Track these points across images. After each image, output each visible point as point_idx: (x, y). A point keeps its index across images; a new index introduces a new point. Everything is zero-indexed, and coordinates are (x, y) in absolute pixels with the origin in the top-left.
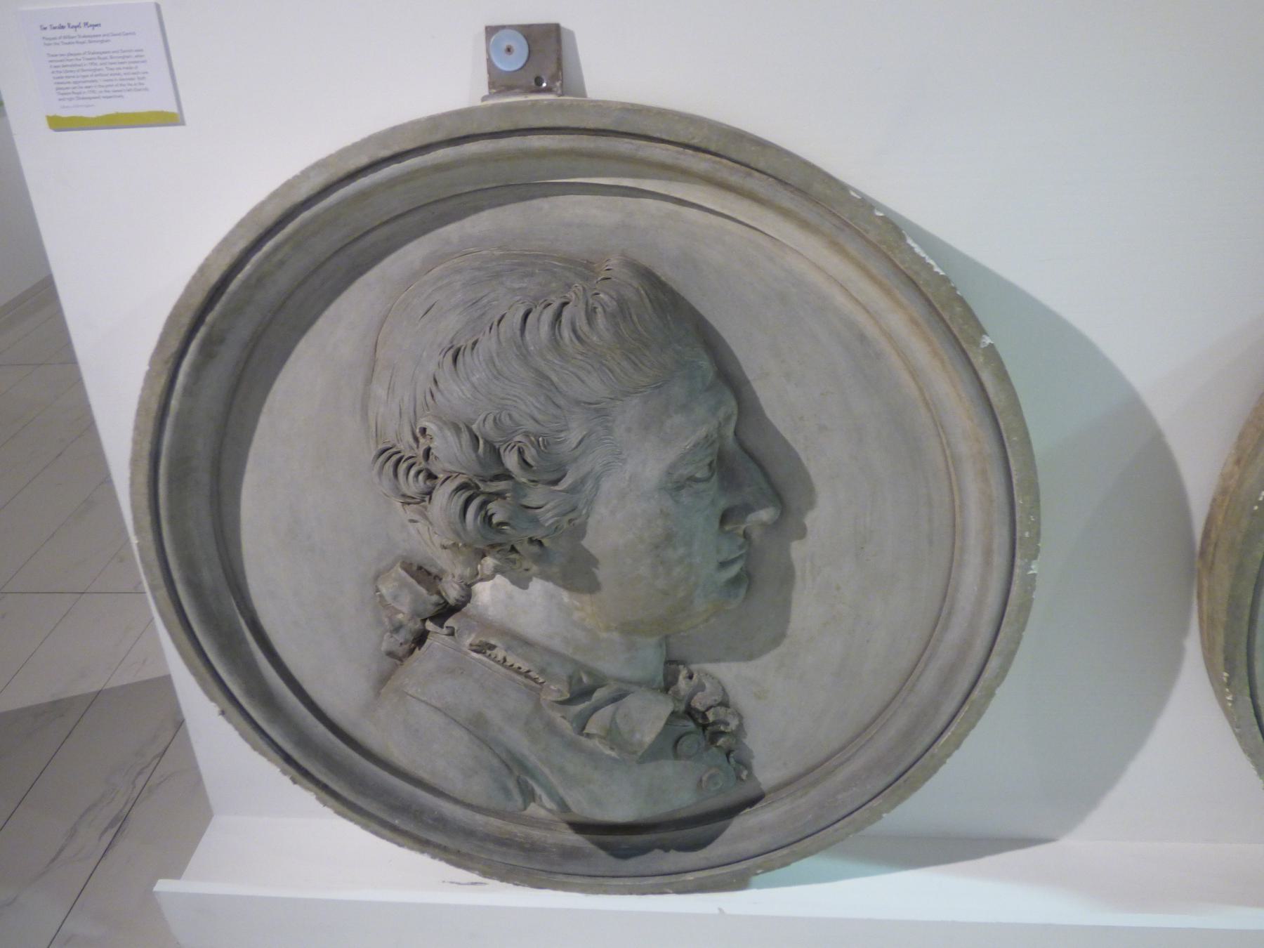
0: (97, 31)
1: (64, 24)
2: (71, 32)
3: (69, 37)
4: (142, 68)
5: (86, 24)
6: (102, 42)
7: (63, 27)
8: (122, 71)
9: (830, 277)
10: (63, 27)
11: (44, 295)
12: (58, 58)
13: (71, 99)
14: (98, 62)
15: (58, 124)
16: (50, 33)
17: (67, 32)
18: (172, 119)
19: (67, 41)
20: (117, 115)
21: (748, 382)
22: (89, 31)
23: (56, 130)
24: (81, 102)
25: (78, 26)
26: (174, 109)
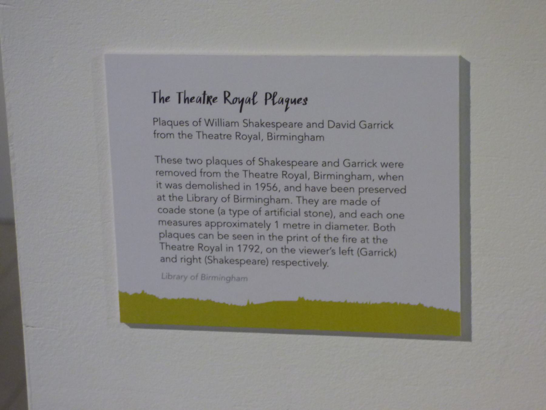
0: (296, 113)
1: (216, 92)
2: (230, 112)
3: (220, 123)
4: (390, 203)
5: (271, 97)
6: (302, 139)
7: (209, 100)
8: (337, 209)
9: (207, 187)
10: (209, 100)
11: (10, 224)
12: (184, 167)
13: (190, 261)
14: (281, 183)
15: (142, 311)
16: (174, 110)
17: (220, 110)
18: (450, 326)
19: (209, 130)
20: (302, 304)
21: (376, 303)
22: (276, 113)
23: (133, 325)
24: (216, 269)
25: (252, 100)
26: (456, 307)
